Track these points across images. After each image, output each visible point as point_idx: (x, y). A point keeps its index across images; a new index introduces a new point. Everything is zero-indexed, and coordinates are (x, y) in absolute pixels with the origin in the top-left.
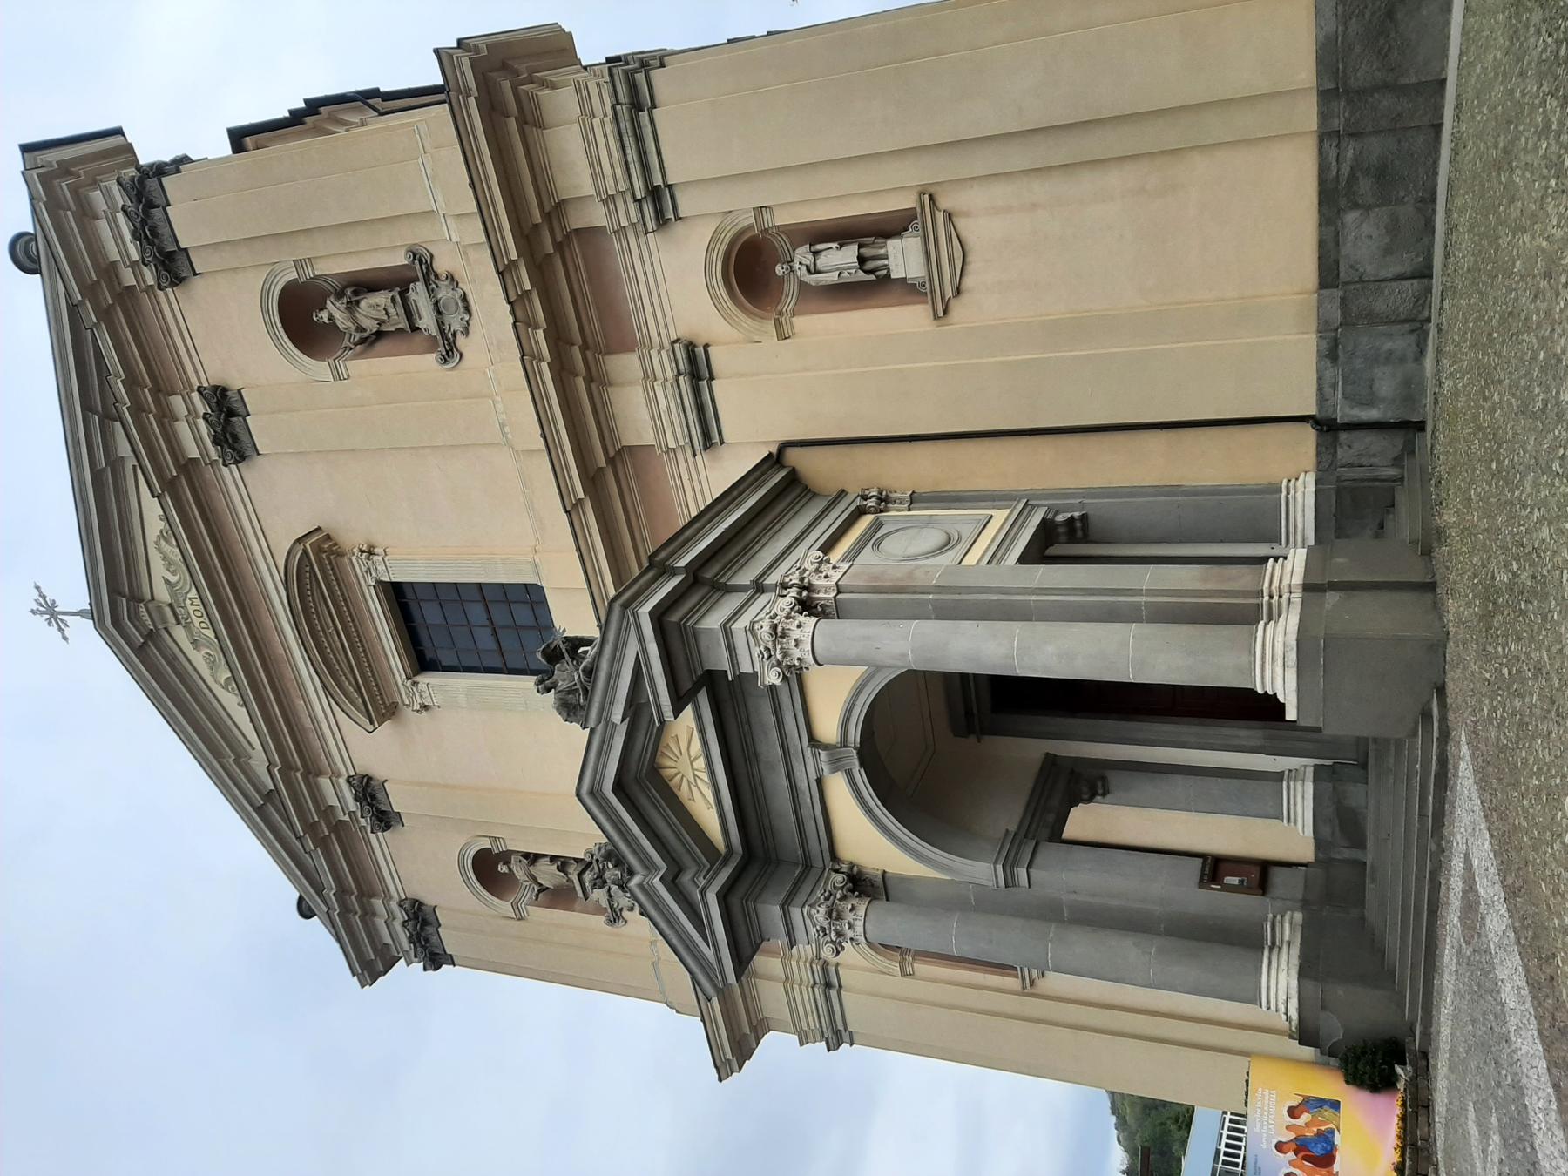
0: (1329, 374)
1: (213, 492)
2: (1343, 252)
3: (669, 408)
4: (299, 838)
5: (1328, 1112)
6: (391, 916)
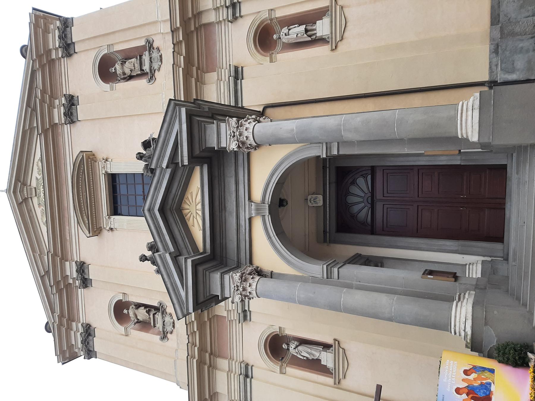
0: (494, 63)
1: (59, 137)
2: (501, 10)
3: (224, 92)
4: (51, 286)
5: (487, 374)
6: (77, 330)
